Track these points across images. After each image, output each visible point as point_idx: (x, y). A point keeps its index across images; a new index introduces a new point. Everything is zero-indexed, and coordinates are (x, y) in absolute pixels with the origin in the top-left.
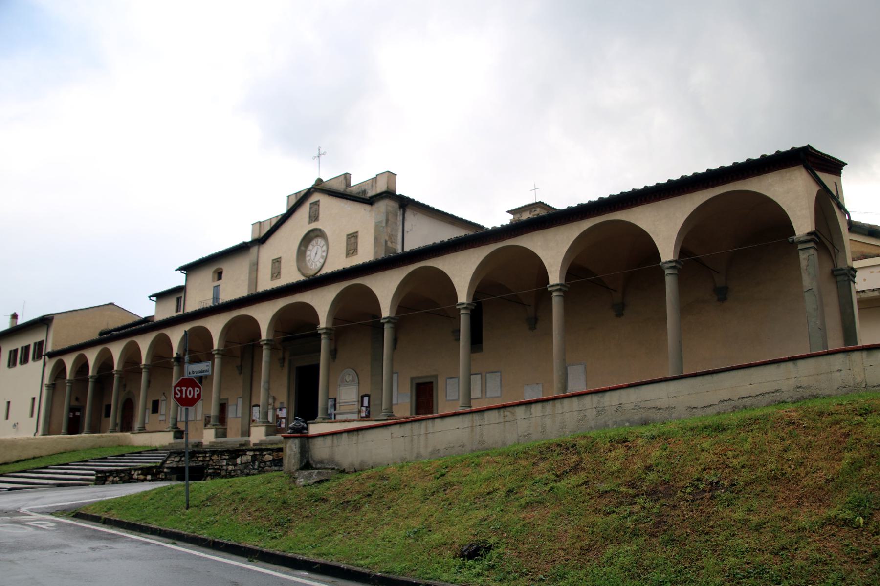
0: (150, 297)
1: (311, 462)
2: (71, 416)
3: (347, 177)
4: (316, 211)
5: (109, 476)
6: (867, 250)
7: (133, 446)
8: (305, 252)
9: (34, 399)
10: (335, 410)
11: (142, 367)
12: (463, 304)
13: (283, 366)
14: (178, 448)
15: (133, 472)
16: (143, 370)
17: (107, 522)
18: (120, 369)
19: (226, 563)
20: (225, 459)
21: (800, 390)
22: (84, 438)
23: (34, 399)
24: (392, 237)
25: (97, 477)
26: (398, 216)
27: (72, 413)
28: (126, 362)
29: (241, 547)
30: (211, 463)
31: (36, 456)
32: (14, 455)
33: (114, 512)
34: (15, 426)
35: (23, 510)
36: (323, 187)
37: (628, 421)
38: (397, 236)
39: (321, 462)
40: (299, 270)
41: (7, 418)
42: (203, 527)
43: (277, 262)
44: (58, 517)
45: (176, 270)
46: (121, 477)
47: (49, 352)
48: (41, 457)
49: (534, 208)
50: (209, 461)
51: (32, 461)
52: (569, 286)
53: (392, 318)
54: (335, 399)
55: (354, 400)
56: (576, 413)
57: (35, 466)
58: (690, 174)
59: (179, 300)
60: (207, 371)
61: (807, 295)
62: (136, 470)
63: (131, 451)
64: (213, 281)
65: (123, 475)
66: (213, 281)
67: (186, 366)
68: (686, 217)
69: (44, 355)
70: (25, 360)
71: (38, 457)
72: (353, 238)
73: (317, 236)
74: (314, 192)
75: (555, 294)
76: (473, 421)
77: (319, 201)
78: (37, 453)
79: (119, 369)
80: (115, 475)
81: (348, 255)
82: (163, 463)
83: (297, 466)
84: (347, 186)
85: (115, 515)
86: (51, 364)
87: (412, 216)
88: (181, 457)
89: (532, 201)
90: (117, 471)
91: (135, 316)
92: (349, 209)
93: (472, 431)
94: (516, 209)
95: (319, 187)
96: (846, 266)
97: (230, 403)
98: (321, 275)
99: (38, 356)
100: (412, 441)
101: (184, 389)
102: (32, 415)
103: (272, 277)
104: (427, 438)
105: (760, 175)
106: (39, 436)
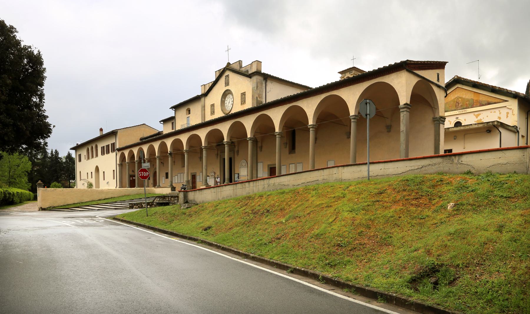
0: (160, 122)
1: (188, 201)
2: (131, 179)
3: (240, 62)
4: (228, 80)
5: (134, 206)
6: (490, 100)
7: (155, 194)
8: (224, 101)
9: (114, 171)
10: (239, 179)
11: (156, 157)
12: (277, 133)
13: (218, 158)
14: (172, 195)
15: (143, 204)
16: (185, 153)
17: (123, 221)
18: (148, 158)
19: (210, 252)
20: (176, 200)
21: (324, 180)
22: (136, 190)
23: (114, 171)
24: (260, 96)
25: (130, 206)
26: (263, 84)
27: (131, 178)
28: (150, 155)
29: (155, 228)
30: (171, 201)
31: (112, 197)
32: (103, 196)
33: (125, 217)
34: (107, 183)
35: (97, 216)
36: (230, 68)
37: (276, 189)
38: (262, 95)
39: (191, 201)
40: (222, 110)
41: (104, 180)
42: (148, 222)
43: (213, 106)
44: (108, 219)
45: (170, 109)
46: (138, 206)
47: (117, 148)
48: (115, 197)
49: (351, 70)
50: (170, 200)
51: (110, 199)
52: (317, 125)
53: (251, 138)
54: (239, 174)
55: (246, 175)
56: (262, 185)
57: (111, 201)
58: (393, 63)
59: (173, 123)
60: (149, 166)
61: (401, 133)
62: (144, 203)
63: (152, 196)
64: (187, 115)
65: (139, 205)
66: (187, 115)
67: (142, 164)
68: (360, 94)
69: (116, 150)
70: (108, 152)
71: (113, 198)
72: (244, 95)
73: (229, 93)
74: (226, 70)
75: (311, 129)
76: (234, 187)
77: (229, 75)
78: (113, 196)
79: (147, 158)
80: (136, 205)
81: (242, 104)
82: (154, 201)
83: (183, 202)
84: (240, 68)
85: (125, 219)
86: (119, 154)
87: (270, 84)
88: (160, 198)
89: (351, 67)
90: (137, 203)
91: (156, 130)
92: (241, 80)
93: (234, 191)
94: (343, 71)
95: (229, 68)
96: (439, 116)
97: (197, 174)
98: (232, 113)
99: (113, 150)
100: (217, 194)
101: (142, 173)
102: (114, 179)
103: (211, 114)
104: (221, 193)
105: (389, 74)
106: (118, 188)
